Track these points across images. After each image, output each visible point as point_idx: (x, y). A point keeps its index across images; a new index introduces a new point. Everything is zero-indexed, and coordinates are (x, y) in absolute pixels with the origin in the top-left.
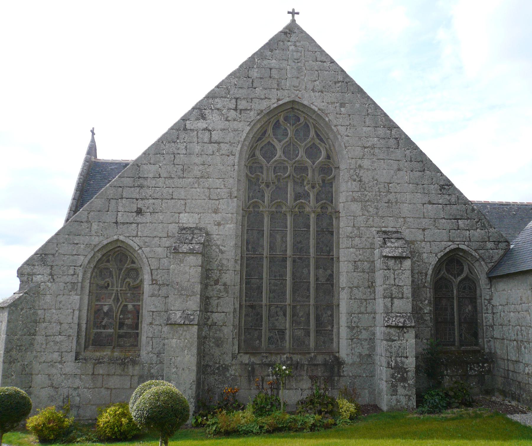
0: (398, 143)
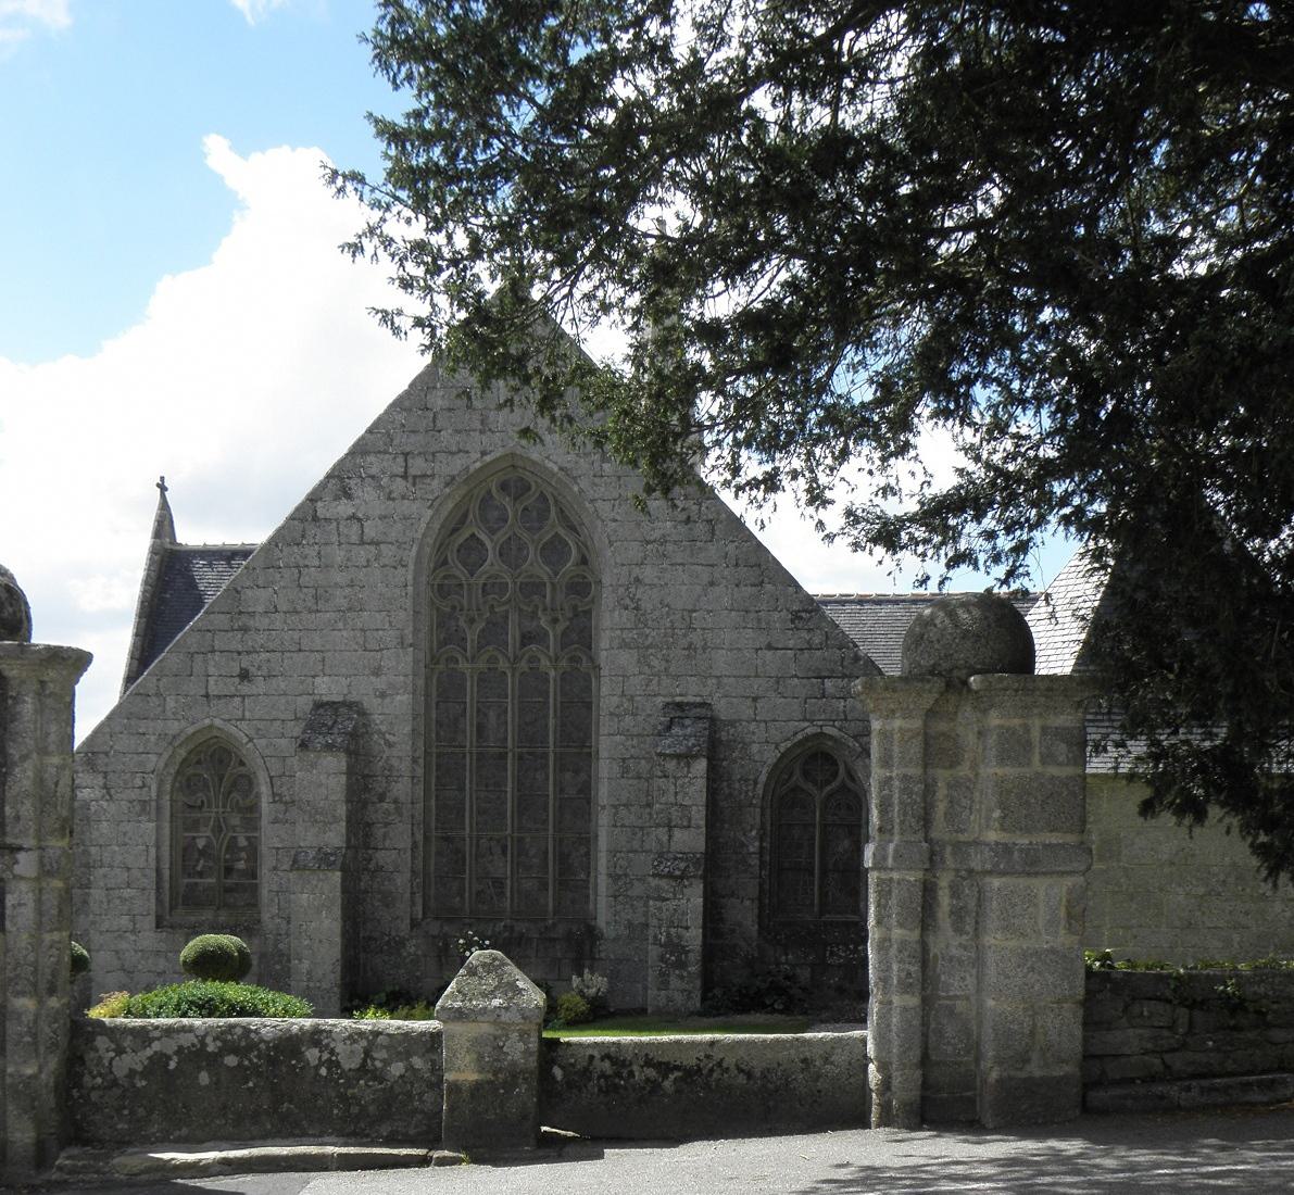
0: (713, 530)
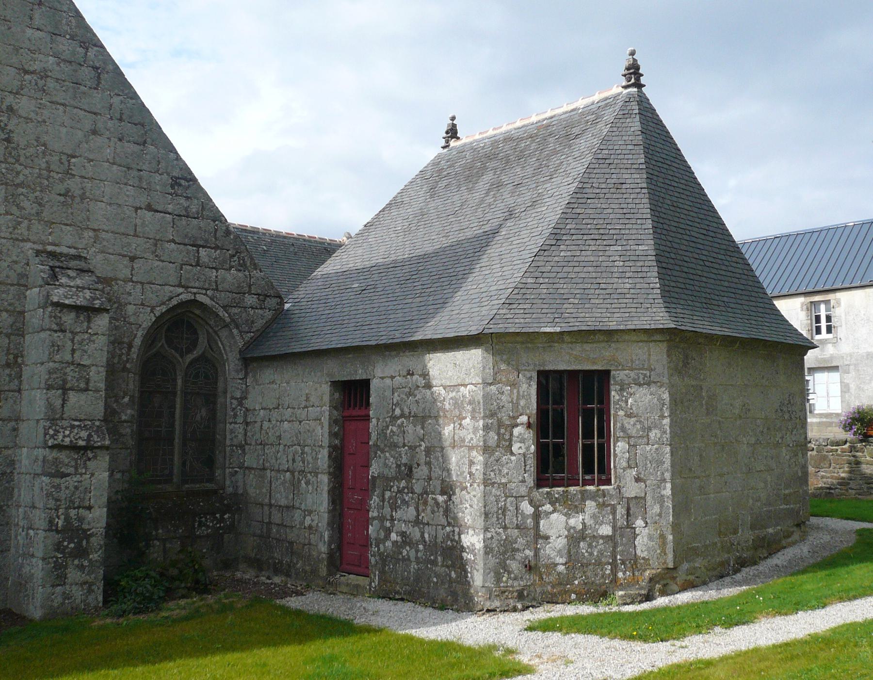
0: (99, 77)
